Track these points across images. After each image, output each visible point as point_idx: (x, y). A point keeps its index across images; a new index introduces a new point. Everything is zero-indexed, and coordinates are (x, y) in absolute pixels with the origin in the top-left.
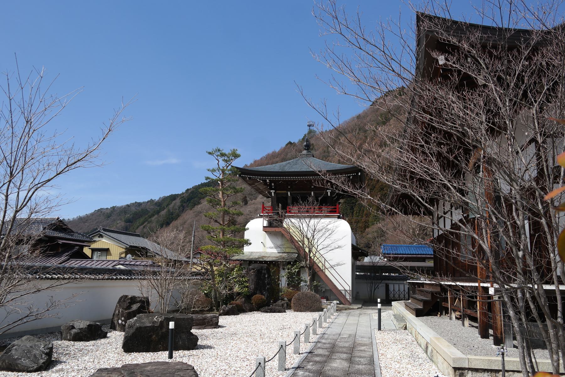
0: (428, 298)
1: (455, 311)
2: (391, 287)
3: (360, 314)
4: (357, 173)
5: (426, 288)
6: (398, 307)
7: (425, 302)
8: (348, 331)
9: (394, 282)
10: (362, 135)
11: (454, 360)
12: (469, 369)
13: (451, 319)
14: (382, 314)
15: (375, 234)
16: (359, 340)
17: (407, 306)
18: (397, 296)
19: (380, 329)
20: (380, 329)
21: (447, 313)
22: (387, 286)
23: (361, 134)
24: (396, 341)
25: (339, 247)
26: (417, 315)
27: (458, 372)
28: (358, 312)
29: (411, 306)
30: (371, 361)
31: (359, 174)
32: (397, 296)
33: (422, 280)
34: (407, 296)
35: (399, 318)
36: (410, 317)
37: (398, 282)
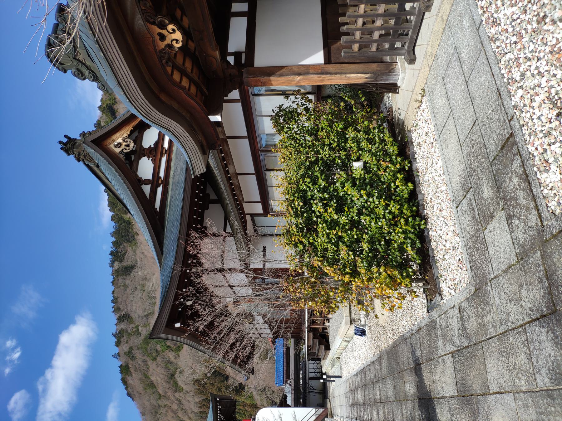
0: (317, 341)
1: (324, 323)
2: (312, 375)
3: (334, 397)
4: (217, 401)
5: (311, 344)
6: (326, 367)
7: (320, 343)
8: (343, 398)
9: (307, 373)
10: (163, 410)
11: (347, 324)
12: (350, 316)
13: (329, 326)
14: (330, 375)
15: (264, 397)
16: (348, 389)
17: (324, 358)
18: (318, 370)
19: (340, 377)
20: (340, 377)
21: (326, 329)
22: (311, 378)
23: (161, 411)
24: (346, 363)
25: (280, 417)
26: (329, 349)
27: (353, 322)
28: (332, 400)
29: (324, 355)
30: (356, 375)
31: (218, 399)
32: (318, 370)
33: (305, 350)
34: (318, 362)
35: (333, 364)
36: (331, 354)
37: (307, 369)
